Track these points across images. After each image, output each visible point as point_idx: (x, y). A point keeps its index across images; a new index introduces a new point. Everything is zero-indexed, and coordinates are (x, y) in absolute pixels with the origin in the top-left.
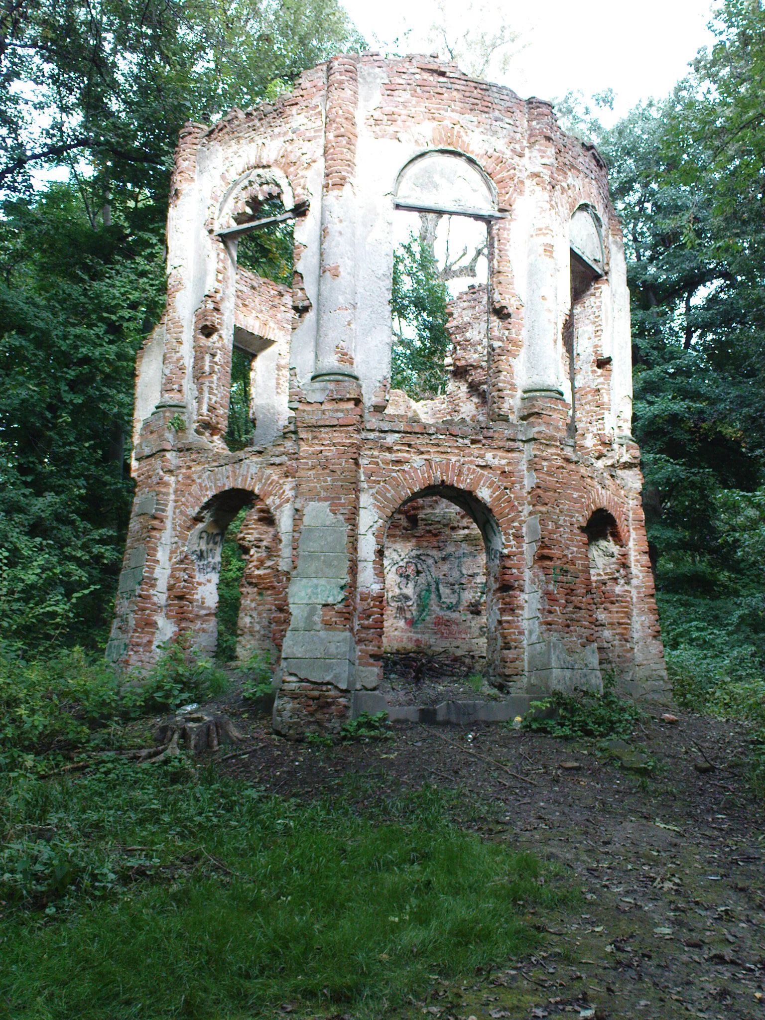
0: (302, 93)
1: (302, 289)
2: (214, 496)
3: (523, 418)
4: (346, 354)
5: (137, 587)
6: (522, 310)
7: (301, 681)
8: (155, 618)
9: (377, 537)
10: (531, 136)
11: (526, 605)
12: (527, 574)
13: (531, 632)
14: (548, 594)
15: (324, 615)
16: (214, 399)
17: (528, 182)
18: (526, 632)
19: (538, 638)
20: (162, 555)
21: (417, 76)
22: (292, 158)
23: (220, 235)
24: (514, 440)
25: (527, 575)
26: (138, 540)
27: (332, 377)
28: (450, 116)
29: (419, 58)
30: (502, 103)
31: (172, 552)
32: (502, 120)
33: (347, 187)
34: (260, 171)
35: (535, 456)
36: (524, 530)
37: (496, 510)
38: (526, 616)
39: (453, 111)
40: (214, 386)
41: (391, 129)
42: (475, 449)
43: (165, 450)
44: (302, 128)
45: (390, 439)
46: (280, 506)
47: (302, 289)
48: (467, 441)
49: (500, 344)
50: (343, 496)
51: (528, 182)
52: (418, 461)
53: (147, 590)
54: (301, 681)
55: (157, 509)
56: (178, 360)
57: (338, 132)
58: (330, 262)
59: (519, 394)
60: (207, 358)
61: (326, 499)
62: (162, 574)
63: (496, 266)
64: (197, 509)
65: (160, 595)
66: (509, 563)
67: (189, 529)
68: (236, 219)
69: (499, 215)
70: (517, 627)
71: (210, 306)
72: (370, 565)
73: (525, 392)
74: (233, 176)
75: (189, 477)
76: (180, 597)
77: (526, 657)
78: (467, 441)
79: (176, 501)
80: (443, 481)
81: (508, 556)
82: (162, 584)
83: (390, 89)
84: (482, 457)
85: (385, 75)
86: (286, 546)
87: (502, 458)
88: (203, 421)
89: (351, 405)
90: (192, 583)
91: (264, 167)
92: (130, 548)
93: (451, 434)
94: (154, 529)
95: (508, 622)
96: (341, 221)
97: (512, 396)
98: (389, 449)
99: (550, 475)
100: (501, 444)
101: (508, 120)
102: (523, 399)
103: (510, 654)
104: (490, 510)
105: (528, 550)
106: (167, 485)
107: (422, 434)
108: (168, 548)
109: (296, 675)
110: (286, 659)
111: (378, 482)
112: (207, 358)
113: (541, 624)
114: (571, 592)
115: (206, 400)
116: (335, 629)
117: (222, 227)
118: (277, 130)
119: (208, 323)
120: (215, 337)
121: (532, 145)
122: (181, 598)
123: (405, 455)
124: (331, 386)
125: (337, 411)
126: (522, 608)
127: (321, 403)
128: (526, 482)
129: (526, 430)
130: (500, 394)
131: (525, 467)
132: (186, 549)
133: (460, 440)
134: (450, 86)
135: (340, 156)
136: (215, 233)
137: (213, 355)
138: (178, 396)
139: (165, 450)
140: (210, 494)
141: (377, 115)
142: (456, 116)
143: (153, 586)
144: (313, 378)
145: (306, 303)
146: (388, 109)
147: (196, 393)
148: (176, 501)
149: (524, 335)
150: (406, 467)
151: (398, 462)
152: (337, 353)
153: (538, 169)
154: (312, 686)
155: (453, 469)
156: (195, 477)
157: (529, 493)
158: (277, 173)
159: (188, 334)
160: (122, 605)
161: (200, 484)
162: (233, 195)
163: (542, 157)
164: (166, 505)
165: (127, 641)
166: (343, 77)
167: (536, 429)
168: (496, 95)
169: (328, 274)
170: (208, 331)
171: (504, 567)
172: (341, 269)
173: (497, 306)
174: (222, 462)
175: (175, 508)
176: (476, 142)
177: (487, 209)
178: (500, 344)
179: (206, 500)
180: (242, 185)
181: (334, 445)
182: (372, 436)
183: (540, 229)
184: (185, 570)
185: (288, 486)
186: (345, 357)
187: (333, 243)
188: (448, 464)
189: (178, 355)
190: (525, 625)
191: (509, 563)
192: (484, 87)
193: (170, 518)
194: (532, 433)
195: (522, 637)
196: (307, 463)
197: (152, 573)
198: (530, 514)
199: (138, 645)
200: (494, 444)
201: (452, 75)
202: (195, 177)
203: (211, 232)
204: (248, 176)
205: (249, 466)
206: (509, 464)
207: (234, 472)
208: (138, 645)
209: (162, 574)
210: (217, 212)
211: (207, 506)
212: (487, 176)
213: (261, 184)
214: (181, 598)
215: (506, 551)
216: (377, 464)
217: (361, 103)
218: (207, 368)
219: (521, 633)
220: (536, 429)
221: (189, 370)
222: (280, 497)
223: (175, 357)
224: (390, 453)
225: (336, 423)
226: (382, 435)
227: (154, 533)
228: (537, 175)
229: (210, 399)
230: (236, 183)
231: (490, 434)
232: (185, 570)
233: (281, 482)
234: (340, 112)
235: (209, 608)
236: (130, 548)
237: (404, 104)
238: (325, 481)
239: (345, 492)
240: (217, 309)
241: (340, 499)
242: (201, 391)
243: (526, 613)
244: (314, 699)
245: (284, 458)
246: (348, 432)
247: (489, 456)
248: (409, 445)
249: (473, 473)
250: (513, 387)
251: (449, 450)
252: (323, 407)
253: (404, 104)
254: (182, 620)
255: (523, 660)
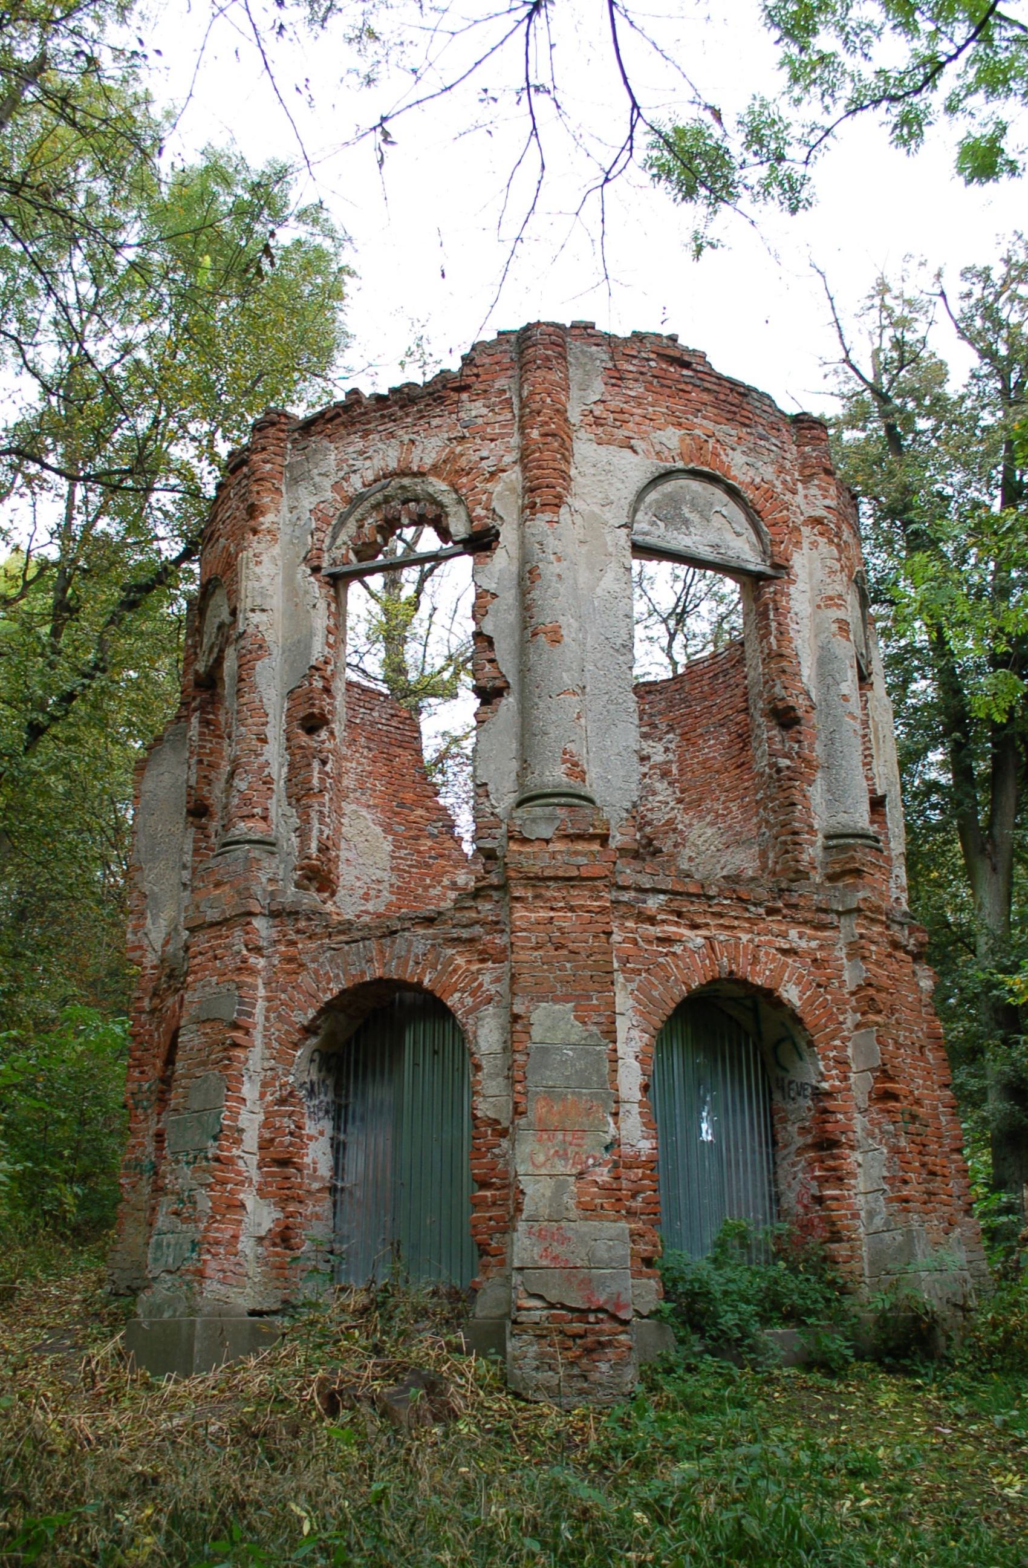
0: (475, 371)
1: (492, 661)
2: (343, 992)
3: (832, 878)
4: (575, 764)
5: (210, 1143)
6: (814, 715)
7: (552, 1306)
8: (242, 1196)
9: (641, 1062)
10: (804, 466)
11: (859, 1170)
12: (857, 1121)
13: (871, 1214)
14: (896, 1150)
15: (580, 1194)
16: (327, 832)
17: (806, 530)
18: (863, 1214)
19: (887, 1223)
20: (249, 1090)
21: (652, 364)
22: (463, 462)
23: (330, 575)
24: (825, 911)
25: (859, 1122)
26: (204, 1063)
27: (563, 800)
28: (703, 425)
29: (653, 339)
30: (764, 415)
31: (264, 1085)
32: (767, 440)
33: (563, 510)
34: (406, 481)
35: (862, 936)
36: (850, 1052)
37: (808, 1019)
38: (861, 1188)
39: (704, 418)
40: (326, 810)
41: (621, 433)
42: (773, 924)
43: (251, 914)
44: (480, 421)
45: (653, 903)
46: (474, 1009)
47: (492, 661)
48: (762, 911)
49: (788, 762)
50: (595, 995)
51: (806, 530)
52: (696, 939)
53: (229, 1150)
54: (552, 1306)
55: (240, 1013)
56: (261, 768)
57: (546, 429)
58: (544, 619)
59: (820, 840)
60: (316, 765)
61: (566, 999)
62: (250, 1121)
63: (775, 647)
64: (311, 1013)
65: (247, 1157)
66: (829, 1104)
67: (296, 1046)
68: (357, 553)
69: (769, 571)
70: (849, 1207)
71: (318, 684)
72: (635, 1109)
73: (828, 837)
74: (356, 484)
75: (291, 960)
76: (281, 1161)
77: (864, 1252)
78: (762, 911)
79: (269, 999)
80: (731, 972)
81: (829, 1095)
82: (251, 1141)
83: (616, 378)
84: (784, 935)
85: (605, 357)
86: (490, 1076)
87: (811, 938)
88: (311, 868)
89: (596, 847)
90: (301, 1137)
91: (414, 475)
92: (184, 1076)
93: (739, 899)
94: (235, 1045)
95: (835, 1198)
96: (559, 560)
97: (813, 844)
98: (652, 920)
99: (880, 967)
100: (809, 916)
101: (774, 440)
102: (826, 848)
103: (841, 1250)
104: (799, 1021)
105: (860, 1084)
106: (253, 971)
107: (698, 896)
108: (258, 1080)
109: (540, 1297)
110: (521, 1269)
111: (638, 972)
112: (316, 765)
113: (890, 1200)
114: (922, 1149)
115: (315, 833)
116: (600, 1218)
117: (334, 563)
118: (435, 422)
119: (316, 711)
120: (324, 734)
121: (806, 480)
122: (284, 1163)
123: (674, 929)
124: (562, 813)
125: (576, 853)
126: (855, 1176)
127: (547, 841)
128: (846, 976)
129: (844, 895)
130: (797, 838)
131: (842, 954)
132: (291, 1079)
133: (753, 909)
134: (698, 382)
135: (551, 464)
136: (323, 572)
137: (324, 763)
138: (262, 825)
139: (251, 914)
140: (336, 988)
141: (598, 410)
142: (710, 425)
143: (238, 1142)
144: (520, 804)
145: (499, 683)
146: (616, 403)
147: (296, 822)
148: (269, 999)
149: (819, 752)
150: (677, 949)
151: (662, 940)
152: (564, 762)
153: (821, 513)
154: (570, 1316)
155: (745, 955)
156: (305, 959)
157: (853, 994)
158: (438, 486)
159: (275, 730)
160: (181, 1176)
161: (316, 972)
162: (357, 514)
163: (825, 497)
164: (254, 1006)
165: (198, 1237)
166: (550, 352)
167: (861, 895)
168: (757, 404)
169: (542, 638)
170: (314, 723)
171: (825, 1111)
172: (563, 632)
173: (781, 705)
174: (357, 935)
175: (268, 1010)
176: (738, 465)
177: (754, 562)
178: (788, 762)
179: (328, 997)
180: (372, 500)
181: (572, 909)
182: (625, 896)
183: (831, 598)
184: (291, 1115)
185: (488, 978)
186: (576, 771)
187: (550, 592)
188: (737, 945)
189: (262, 759)
190: (860, 1202)
191: (829, 1104)
192: (742, 390)
193: (260, 1028)
194: (855, 899)
195: (858, 1222)
196: (528, 939)
197: (236, 1120)
198: (858, 1026)
199: (217, 1243)
200: (800, 916)
201: (700, 368)
202: (283, 488)
203: (316, 570)
204: (384, 488)
205: (410, 944)
206: (821, 947)
207: (382, 952)
208: (217, 1243)
209: (250, 1121)
210: (327, 541)
211: (327, 1010)
212: (753, 514)
213: (405, 502)
214: (284, 1163)
215: (825, 1085)
216: (635, 942)
217: (574, 393)
218: (315, 782)
219: (855, 1216)
220: (861, 895)
221: (280, 786)
222: (473, 994)
223: (257, 763)
224: (653, 925)
225: (575, 873)
226: (641, 896)
227: (237, 1053)
228: (818, 521)
229: (321, 832)
230: (361, 498)
231: (794, 901)
232: (291, 1115)
233: (474, 967)
234: (548, 400)
235: (322, 1178)
236: (184, 1076)
237: (638, 400)
238: (562, 969)
239: (597, 986)
240: (327, 690)
241: (590, 998)
242: (306, 820)
243: (860, 1183)
244: (574, 1337)
245: (478, 930)
246: (593, 889)
247: (793, 933)
248: (680, 915)
249: (773, 961)
250: (811, 830)
251: (736, 923)
252: (552, 847)
253: (638, 400)
254: (288, 1199)
255: (861, 1258)
